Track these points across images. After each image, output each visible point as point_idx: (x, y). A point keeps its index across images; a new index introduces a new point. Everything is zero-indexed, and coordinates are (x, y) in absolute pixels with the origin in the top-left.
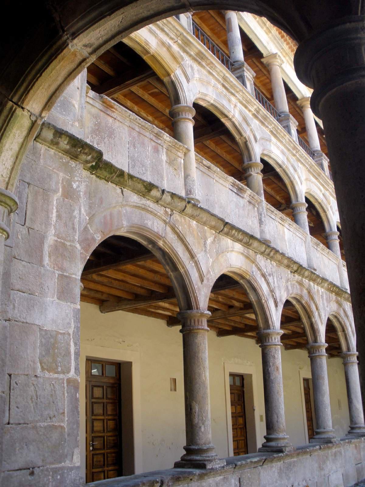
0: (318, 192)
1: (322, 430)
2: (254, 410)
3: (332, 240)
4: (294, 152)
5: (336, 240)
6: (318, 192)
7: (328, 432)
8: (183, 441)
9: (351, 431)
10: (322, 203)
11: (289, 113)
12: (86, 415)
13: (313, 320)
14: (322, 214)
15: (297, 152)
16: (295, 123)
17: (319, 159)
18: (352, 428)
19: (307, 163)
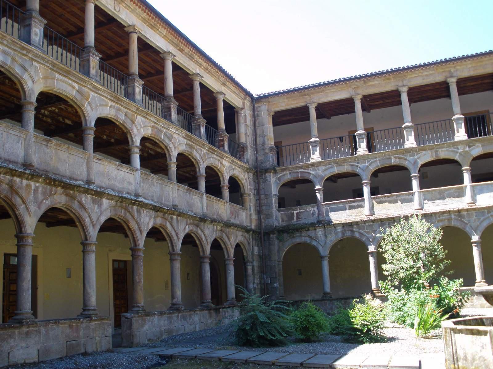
0: (69, 89)
1: (18, 312)
2: (37, 288)
3: (86, 135)
4: (25, 52)
5: (91, 135)
6: (69, 89)
7: (23, 313)
8: (82, 306)
9: (83, 313)
10: (74, 99)
11: (36, 14)
12: (4, 279)
13: (17, 213)
14: (79, 110)
15: (27, 52)
16: (41, 21)
17: (88, 55)
18: (84, 310)
19: (47, 62)
